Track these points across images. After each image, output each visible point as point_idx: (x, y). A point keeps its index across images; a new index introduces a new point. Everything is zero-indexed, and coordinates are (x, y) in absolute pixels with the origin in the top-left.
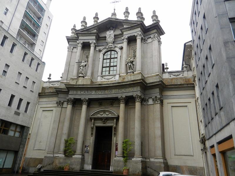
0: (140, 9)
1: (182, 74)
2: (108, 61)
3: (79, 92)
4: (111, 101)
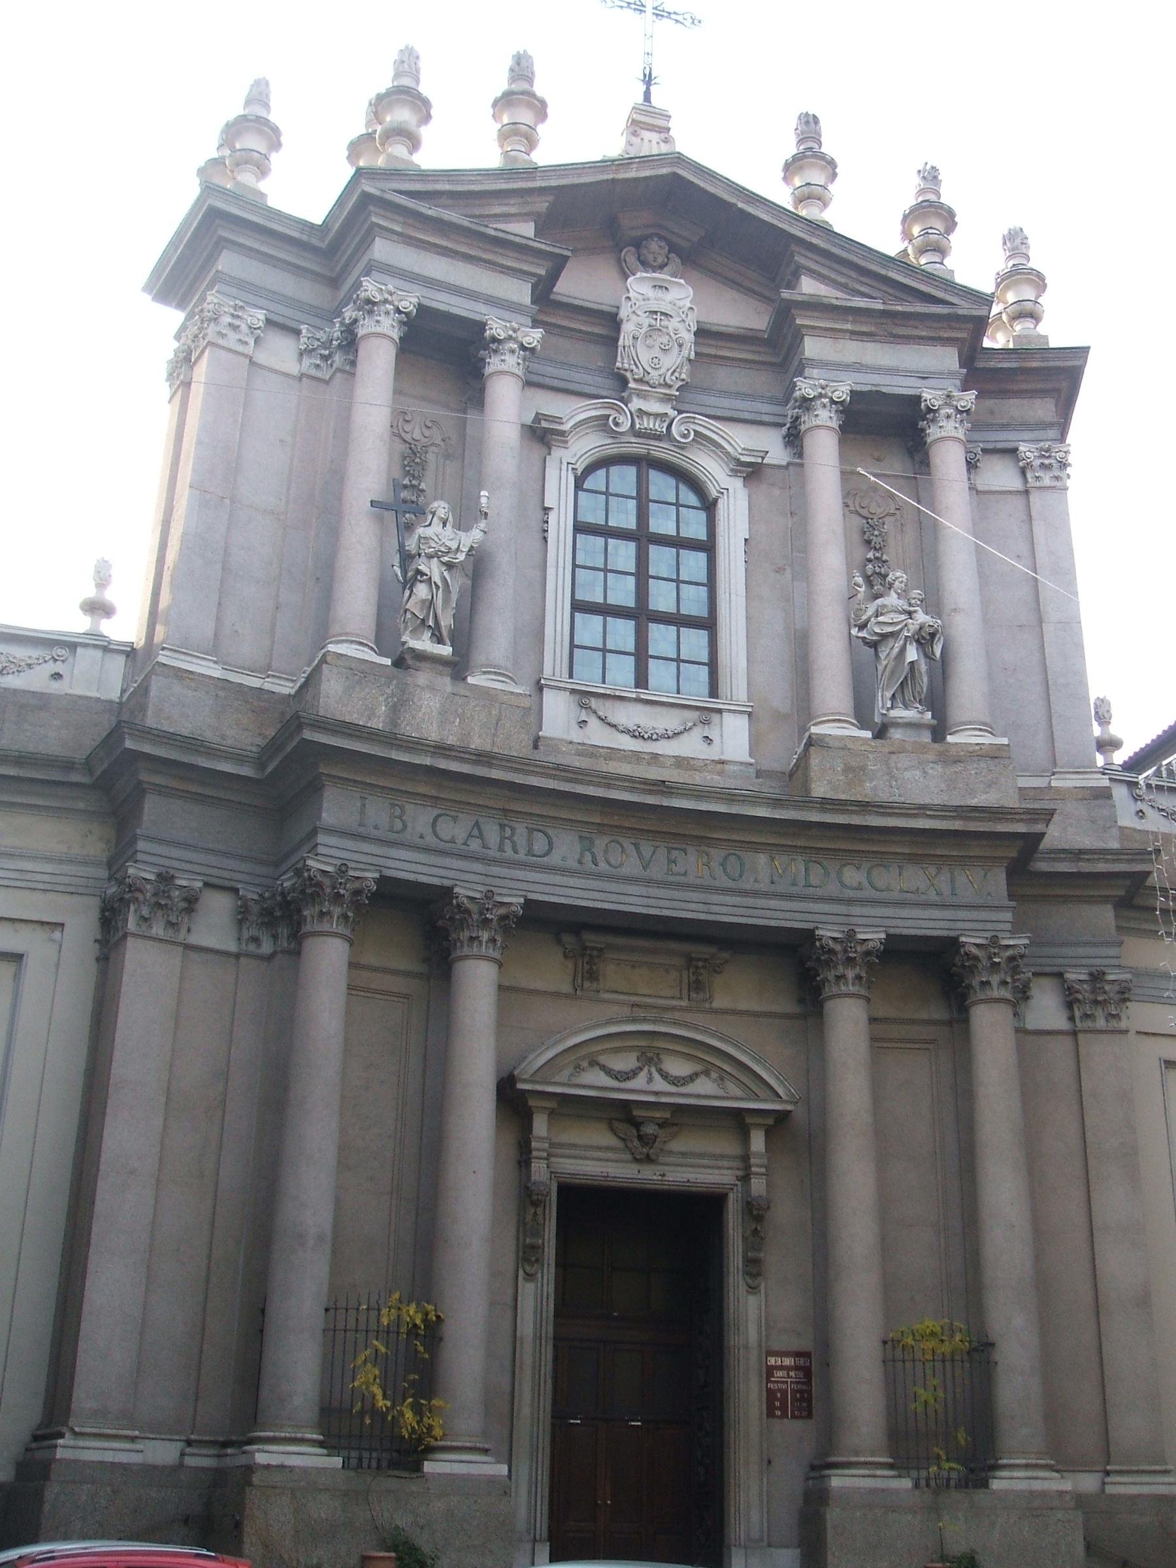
0: (931, 177)
1: (52, 667)
2: (661, 559)
3: (420, 820)
4: (706, 950)
